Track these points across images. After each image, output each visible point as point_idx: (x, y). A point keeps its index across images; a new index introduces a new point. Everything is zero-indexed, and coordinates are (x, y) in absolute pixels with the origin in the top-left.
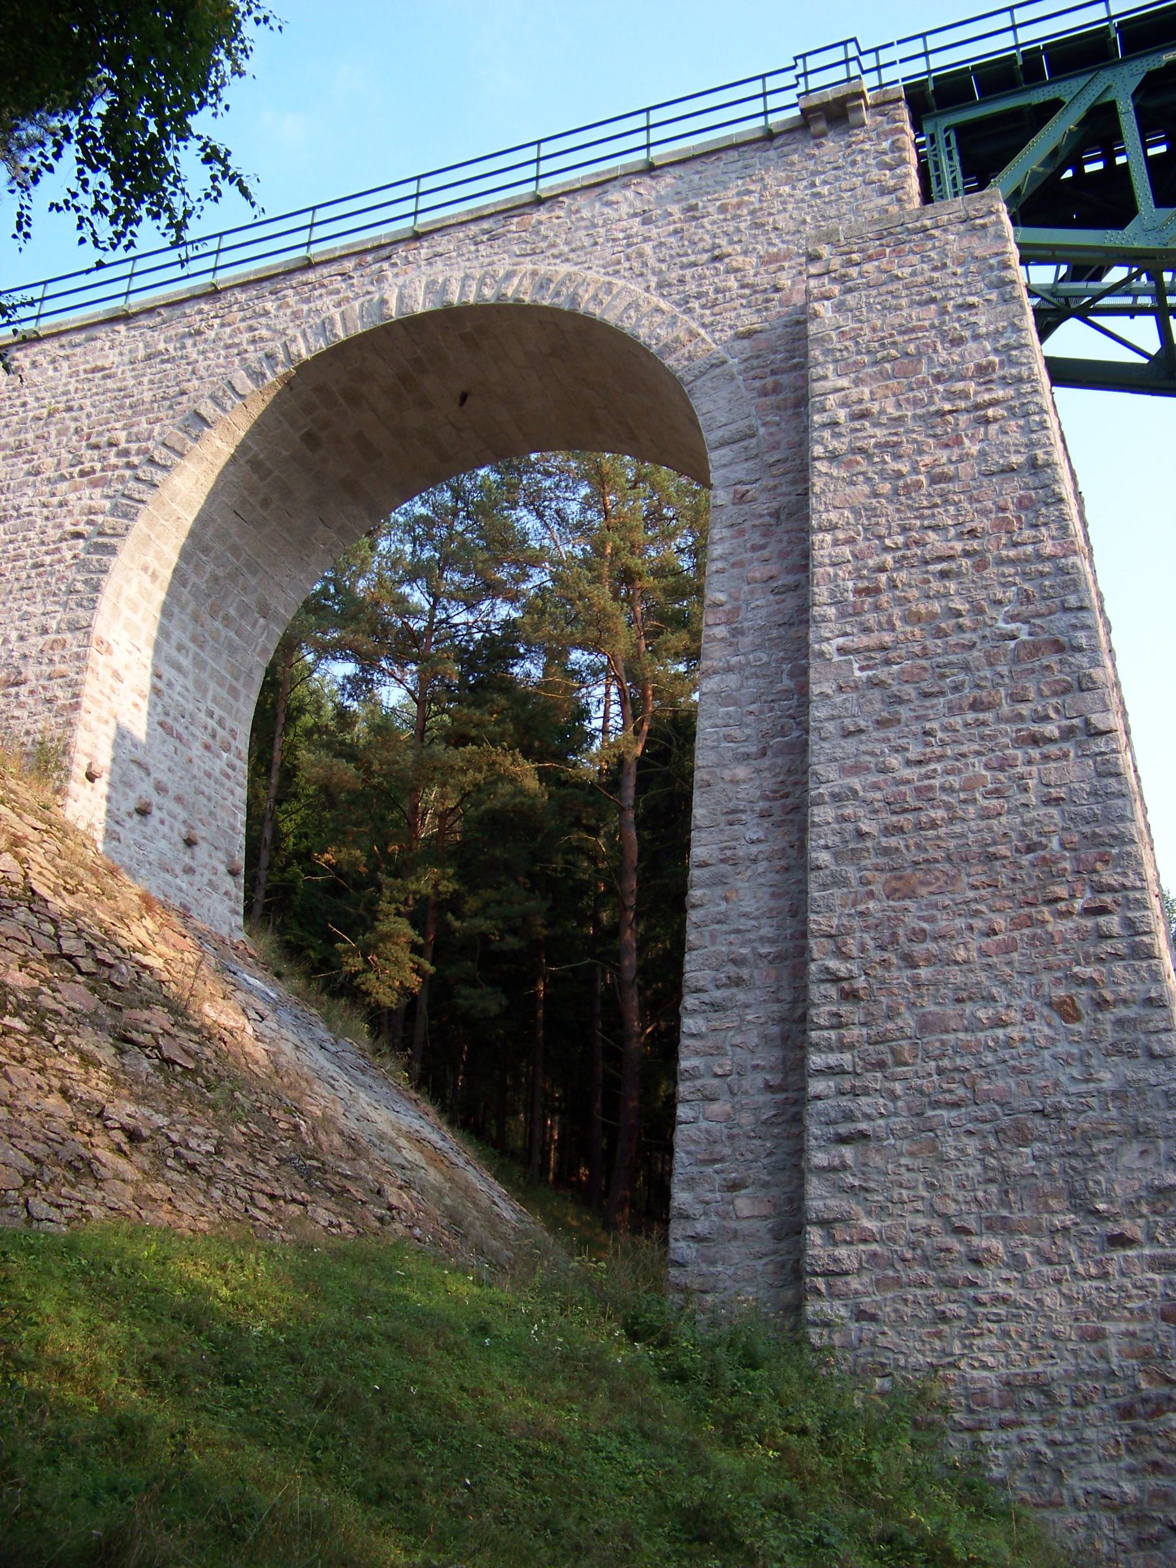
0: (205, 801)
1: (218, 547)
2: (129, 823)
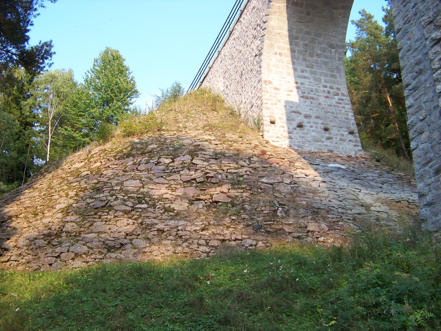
0: (331, 114)
1: (300, 35)
2: (295, 132)
